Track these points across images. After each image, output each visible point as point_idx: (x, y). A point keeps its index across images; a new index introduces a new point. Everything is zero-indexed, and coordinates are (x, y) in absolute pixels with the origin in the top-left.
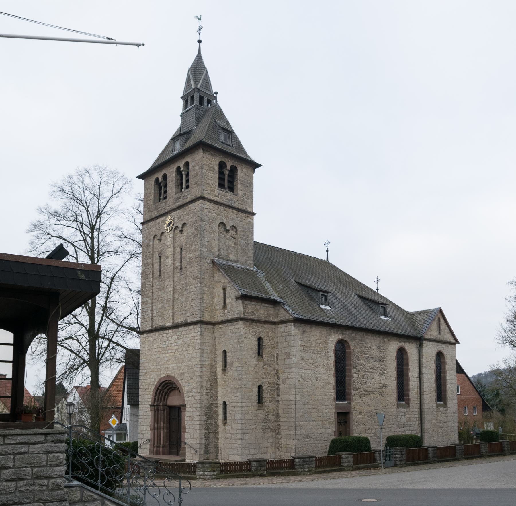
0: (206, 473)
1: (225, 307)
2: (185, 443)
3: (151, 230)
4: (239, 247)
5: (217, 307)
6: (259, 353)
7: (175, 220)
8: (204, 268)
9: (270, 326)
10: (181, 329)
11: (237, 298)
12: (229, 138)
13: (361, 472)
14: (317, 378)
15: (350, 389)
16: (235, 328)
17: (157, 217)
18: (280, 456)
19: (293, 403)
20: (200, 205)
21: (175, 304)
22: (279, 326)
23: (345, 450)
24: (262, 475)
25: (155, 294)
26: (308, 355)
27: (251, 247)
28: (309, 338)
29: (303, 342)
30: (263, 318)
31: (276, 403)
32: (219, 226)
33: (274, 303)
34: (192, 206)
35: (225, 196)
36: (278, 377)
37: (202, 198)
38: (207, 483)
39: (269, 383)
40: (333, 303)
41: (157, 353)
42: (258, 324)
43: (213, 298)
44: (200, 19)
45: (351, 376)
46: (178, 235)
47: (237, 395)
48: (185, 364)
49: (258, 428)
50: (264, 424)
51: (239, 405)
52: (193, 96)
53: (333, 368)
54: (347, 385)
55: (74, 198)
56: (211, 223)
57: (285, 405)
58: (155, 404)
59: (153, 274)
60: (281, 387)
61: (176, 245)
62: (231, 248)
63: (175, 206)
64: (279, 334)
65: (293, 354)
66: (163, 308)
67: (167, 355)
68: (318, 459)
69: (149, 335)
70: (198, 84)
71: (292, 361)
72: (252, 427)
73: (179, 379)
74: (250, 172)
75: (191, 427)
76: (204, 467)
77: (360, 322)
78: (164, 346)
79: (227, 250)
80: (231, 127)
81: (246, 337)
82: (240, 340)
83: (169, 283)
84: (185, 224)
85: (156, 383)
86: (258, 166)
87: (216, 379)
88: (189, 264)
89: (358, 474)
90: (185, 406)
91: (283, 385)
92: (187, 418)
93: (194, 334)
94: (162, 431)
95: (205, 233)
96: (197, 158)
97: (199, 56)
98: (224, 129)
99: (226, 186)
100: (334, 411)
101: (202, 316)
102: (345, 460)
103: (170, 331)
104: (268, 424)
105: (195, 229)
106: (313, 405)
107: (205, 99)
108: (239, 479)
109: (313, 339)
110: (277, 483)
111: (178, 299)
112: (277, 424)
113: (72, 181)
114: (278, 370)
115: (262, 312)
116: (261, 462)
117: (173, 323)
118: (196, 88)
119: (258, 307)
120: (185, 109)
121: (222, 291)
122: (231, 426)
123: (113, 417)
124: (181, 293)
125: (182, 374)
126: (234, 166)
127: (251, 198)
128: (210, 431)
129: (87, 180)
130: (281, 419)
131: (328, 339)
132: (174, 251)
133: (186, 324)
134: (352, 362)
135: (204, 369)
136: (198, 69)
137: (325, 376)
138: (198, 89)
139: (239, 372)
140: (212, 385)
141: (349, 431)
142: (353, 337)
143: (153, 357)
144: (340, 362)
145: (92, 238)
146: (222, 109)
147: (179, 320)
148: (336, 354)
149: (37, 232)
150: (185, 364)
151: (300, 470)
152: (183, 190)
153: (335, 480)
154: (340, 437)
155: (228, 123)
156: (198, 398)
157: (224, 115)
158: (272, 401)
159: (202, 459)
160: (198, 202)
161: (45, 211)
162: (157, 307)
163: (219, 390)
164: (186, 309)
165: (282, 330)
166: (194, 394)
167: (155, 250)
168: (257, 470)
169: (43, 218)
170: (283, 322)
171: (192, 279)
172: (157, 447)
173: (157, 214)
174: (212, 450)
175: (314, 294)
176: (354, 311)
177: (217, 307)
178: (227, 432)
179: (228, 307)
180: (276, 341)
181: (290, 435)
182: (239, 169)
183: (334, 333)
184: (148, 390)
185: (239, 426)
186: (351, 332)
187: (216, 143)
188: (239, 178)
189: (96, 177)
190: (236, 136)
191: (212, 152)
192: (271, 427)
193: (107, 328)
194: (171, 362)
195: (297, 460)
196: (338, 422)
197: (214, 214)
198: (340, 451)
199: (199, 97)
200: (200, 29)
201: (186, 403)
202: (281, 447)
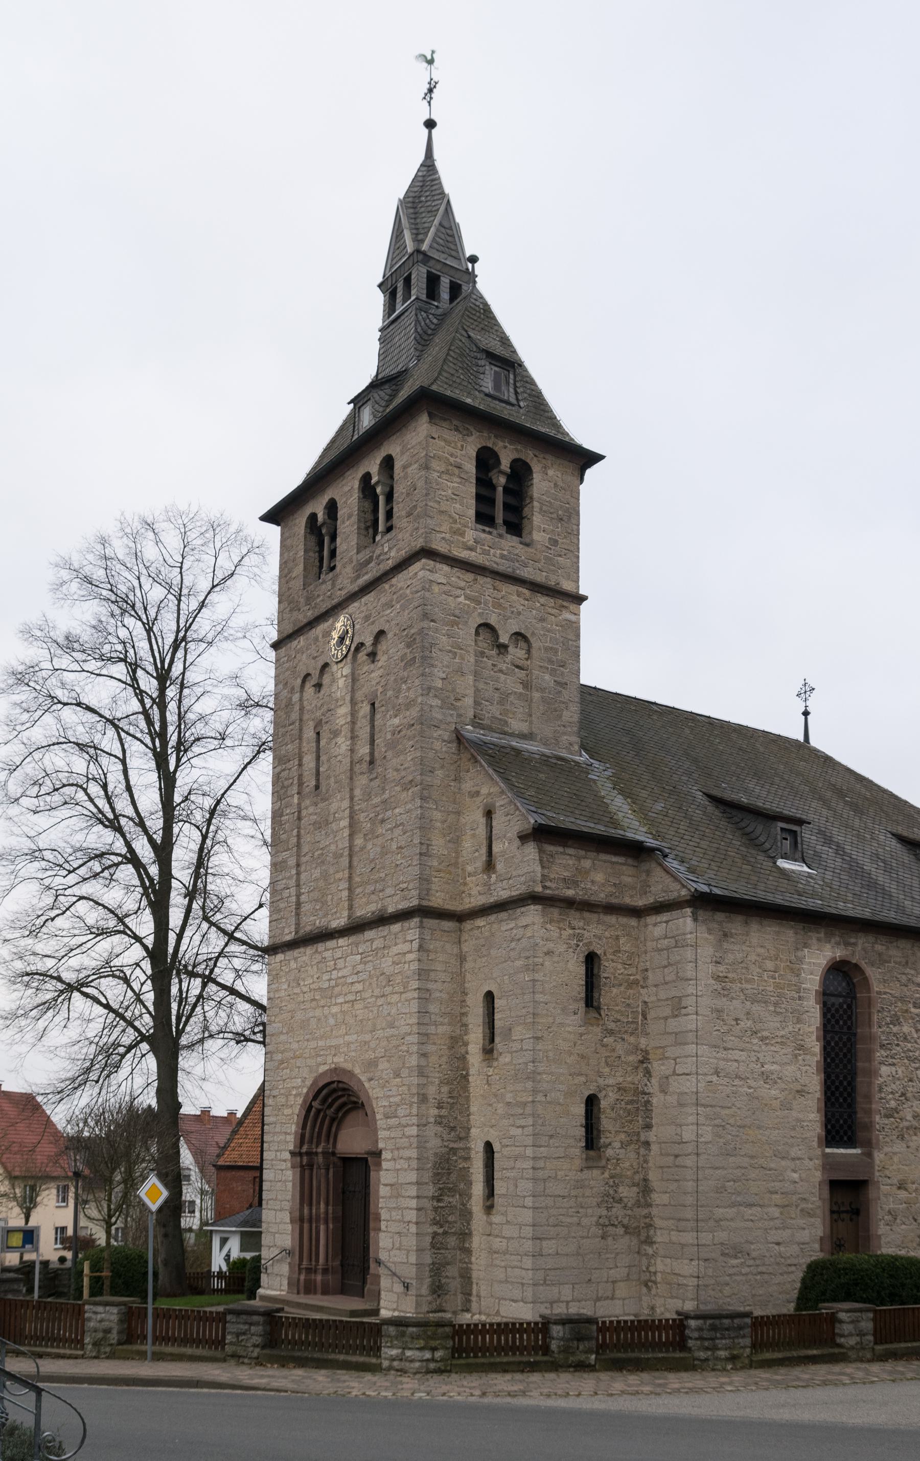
0: (409, 1353)
1: (490, 865)
2: (379, 1262)
3: (296, 661)
4: (536, 695)
5: (469, 869)
6: (591, 1000)
7: (357, 627)
8: (431, 754)
9: (624, 920)
10: (370, 934)
11: (523, 838)
12: (508, 383)
13: (901, 1366)
14: (766, 1077)
15: (869, 1112)
16: (517, 927)
17: (311, 624)
18: (653, 1308)
19: (690, 1148)
20: (421, 574)
21: (355, 863)
22: (651, 919)
23: (849, 1297)
24: (581, 1367)
25: (307, 839)
26: (736, 1006)
27: (571, 694)
28: (739, 956)
29: (721, 968)
30: (601, 897)
31: (642, 1151)
32: (477, 633)
33: (636, 851)
34: (400, 580)
35: (497, 549)
36: (648, 1073)
37: (427, 553)
38: (411, 1388)
39: (620, 1089)
40: (817, 854)
41: (308, 1005)
42: (587, 915)
43: (456, 841)
44: (431, 62)
45: (872, 1073)
46: (365, 668)
47: (522, 1122)
48: (380, 1033)
49: (585, 1221)
50: (604, 1212)
51: (529, 1152)
52: (410, 275)
53: (816, 1048)
54: (859, 1099)
55: (125, 605)
56: (453, 624)
57: (668, 1155)
58: (304, 1149)
59: (301, 784)
60: (654, 1101)
61: (359, 695)
62: (512, 698)
63: (355, 587)
64: (649, 944)
65: (691, 1001)
66: (325, 876)
67: (335, 1009)
68: (760, 1323)
69: (290, 954)
70: (422, 241)
71: (689, 1022)
72: (569, 1220)
73: (363, 1078)
74: (572, 479)
75: (396, 1215)
76: (403, 1334)
77: (901, 909)
78: (326, 985)
79: (501, 702)
80: (514, 352)
81: (549, 953)
82: (531, 961)
83: (339, 804)
84: (381, 633)
85: (305, 1090)
86: (592, 458)
87: (465, 1077)
88: (391, 745)
89: (890, 1373)
90: (378, 1154)
91: (661, 1096)
92: (383, 1191)
93: (403, 947)
94: (322, 1227)
95: (435, 653)
96: (414, 442)
97: (429, 165)
98: (492, 356)
99: (499, 519)
100: (818, 1176)
101: (425, 892)
102: (847, 1328)
103: (342, 942)
104: (617, 1210)
105: (408, 646)
106: (752, 1157)
107: (445, 282)
108: (508, 1376)
109: (753, 957)
110: (623, 1392)
111: (362, 849)
112: (645, 1211)
113: (109, 552)
114: (647, 1052)
115: (599, 877)
116: (579, 1326)
117: (349, 917)
118: (418, 251)
119: (587, 864)
120: (389, 318)
121: (483, 821)
122: (505, 1214)
123: (153, 1180)
124: (372, 831)
125: (372, 1064)
126: (522, 461)
127: (573, 552)
128: (447, 1233)
129: (150, 552)
130: (656, 1198)
131: (800, 960)
132: (353, 713)
133: (383, 920)
134: (875, 1029)
135: (430, 1048)
136: (425, 201)
137: (790, 1071)
138: (424, 253)
139: (529, 1056)
140: (455, 1094)
141: (868, 1238)
142: (880, 954)
143: (299, 1016)
144: (845, 1038)
145: (162, 704)
146: (489, 302)
147: (366, 909)
148: (825, 1004)
149: (23, 695)
150: (380, 1033)
151: (702, 1355)
152: (378, 538)
153: (809, 1392)
154: (835, 1257)
155: (505, 341)
156: (414, 1131)
157: (494, 318)
158: (630, 1143)
159: (425, 1308)
160: (417, 566)
161: (39, 633)
162: (311, 874)
163: (473, 1109)
164: (382, 875)
165: (658, 931)
166: (404, 1121)
167: (306, 717)
168: (566, 1350)
169: (37, 653)
170: (660, 908)
171: (398, 788)
172: (309, 1271)
173: (310, 615)
174: (454, 1285)
175: (758, 828)
176: (881, 878)
177: (469, 869)
178: (496, 1232)
179: (500, 866)
180: (642, 966)
181: (683, 1246)
182: (536, 468)
183: (819, 940)
184: (287, 1111)
185: (527, 1216)
186: (871, 938)
187: (469, 394)
188: (536, 495)
189: (172, 542)
190: (529, 377)
191: (455, 422)
192: (626, 1221)
193: (197, 944)
194: (343, 1031)
195: (693, 1323)
196: (832, 1212)
197: (462, 599)
198: (835, 1300)
199: (429, 276)
200: (430, 91)
201: (381, 1145)
202: (655, 1283)
